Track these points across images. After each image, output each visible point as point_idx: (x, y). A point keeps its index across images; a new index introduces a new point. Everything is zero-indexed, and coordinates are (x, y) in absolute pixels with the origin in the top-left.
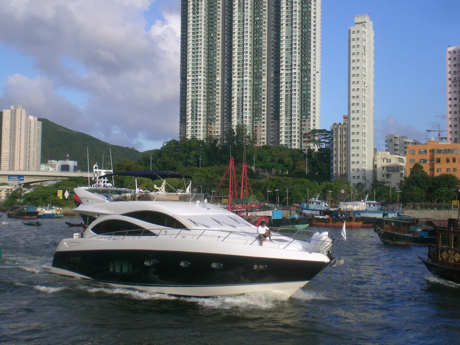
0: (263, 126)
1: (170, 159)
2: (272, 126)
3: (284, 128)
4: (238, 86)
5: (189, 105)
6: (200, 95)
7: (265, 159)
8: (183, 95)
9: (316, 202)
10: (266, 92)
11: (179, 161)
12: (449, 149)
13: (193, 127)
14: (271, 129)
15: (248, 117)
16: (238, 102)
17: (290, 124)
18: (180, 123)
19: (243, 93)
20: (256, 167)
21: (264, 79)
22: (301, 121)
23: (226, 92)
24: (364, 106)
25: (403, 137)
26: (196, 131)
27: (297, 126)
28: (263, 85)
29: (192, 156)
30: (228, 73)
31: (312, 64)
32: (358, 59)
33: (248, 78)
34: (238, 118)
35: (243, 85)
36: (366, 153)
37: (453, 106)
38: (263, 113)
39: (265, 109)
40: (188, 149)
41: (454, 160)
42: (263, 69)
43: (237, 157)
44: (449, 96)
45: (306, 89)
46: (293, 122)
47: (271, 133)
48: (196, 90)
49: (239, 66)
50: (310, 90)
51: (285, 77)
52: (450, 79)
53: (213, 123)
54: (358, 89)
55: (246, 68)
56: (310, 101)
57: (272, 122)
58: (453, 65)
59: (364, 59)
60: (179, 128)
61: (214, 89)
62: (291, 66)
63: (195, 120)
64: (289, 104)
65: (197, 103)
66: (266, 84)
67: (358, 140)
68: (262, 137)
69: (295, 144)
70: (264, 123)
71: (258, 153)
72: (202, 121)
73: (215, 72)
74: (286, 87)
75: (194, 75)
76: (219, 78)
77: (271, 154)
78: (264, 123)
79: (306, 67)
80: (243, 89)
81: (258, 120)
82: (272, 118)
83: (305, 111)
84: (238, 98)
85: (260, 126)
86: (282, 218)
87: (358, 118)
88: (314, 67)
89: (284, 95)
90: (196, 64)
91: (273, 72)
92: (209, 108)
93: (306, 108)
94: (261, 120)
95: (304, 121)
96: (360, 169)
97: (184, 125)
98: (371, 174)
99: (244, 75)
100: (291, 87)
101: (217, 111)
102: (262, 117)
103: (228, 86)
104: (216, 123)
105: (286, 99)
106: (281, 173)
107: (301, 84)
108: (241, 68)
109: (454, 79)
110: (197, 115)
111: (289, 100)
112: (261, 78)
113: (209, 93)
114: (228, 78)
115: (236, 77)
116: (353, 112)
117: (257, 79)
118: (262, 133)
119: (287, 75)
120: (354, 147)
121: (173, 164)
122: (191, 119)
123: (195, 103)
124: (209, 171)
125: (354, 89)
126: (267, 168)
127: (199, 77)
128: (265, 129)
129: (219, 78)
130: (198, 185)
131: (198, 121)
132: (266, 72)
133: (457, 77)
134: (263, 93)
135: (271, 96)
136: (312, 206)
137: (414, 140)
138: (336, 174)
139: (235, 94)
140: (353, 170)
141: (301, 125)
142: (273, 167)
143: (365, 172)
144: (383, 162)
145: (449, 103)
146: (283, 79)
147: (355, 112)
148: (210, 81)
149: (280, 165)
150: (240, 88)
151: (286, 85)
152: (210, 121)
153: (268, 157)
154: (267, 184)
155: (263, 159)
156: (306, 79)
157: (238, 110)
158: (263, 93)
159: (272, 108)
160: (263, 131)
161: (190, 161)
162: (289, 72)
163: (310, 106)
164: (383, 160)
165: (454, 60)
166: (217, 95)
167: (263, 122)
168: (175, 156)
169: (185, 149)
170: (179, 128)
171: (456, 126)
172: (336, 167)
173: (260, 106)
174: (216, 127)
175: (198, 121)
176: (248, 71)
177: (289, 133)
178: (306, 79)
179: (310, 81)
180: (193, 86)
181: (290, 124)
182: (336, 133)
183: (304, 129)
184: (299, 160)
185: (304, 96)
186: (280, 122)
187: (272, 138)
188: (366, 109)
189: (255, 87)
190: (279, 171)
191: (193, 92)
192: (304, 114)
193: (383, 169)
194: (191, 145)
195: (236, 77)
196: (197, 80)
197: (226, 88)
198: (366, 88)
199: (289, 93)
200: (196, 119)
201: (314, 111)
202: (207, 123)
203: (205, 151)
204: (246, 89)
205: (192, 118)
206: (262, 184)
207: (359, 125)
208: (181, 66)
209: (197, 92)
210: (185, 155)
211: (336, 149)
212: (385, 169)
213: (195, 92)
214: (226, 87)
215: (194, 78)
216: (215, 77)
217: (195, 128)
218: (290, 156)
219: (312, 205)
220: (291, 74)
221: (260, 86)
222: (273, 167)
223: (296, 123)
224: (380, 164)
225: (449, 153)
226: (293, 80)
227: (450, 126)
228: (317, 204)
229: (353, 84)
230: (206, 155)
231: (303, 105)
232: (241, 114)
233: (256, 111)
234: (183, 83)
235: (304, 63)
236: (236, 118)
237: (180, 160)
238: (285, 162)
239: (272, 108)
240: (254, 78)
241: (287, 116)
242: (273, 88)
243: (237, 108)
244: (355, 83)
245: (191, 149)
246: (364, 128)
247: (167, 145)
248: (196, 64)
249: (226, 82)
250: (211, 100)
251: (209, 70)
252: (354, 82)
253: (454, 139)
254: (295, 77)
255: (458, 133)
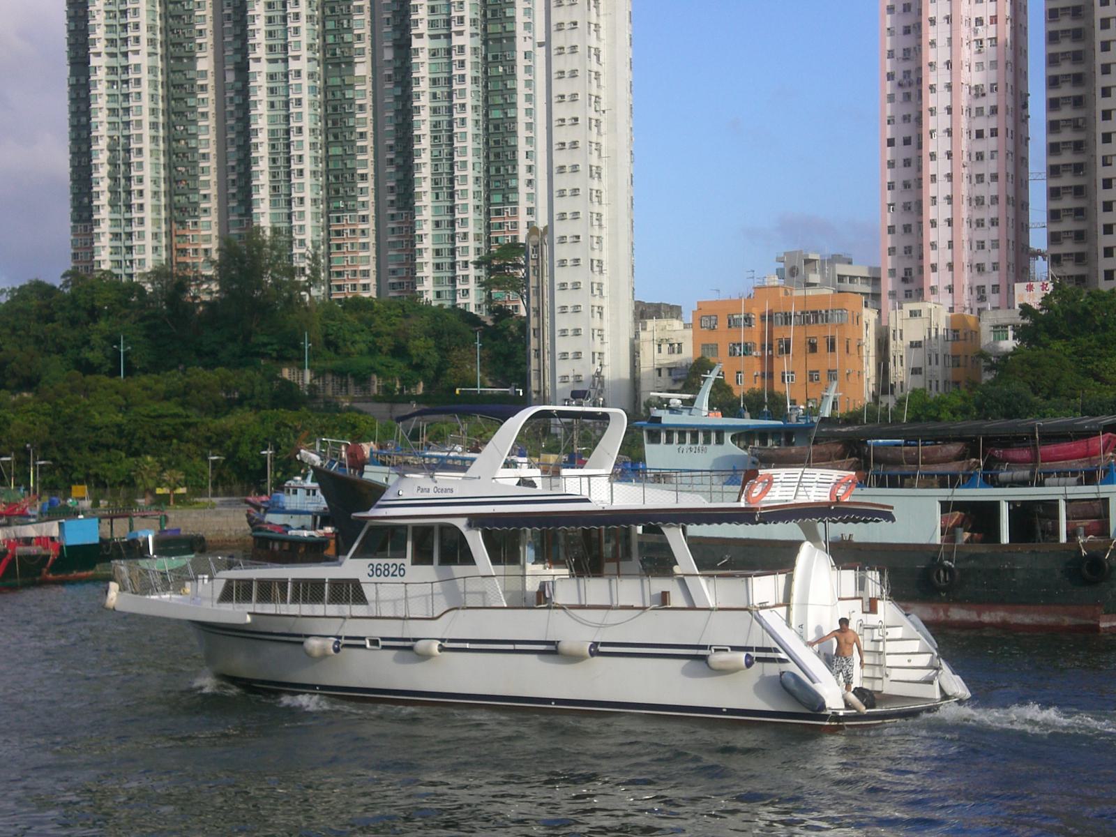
0: (363, 231)
1: (21, 350)
2: (393, 229)
3: (430, 237)
4: (272, 91)
5: (101, 156)
6: (139, 124)
7: (349, 344)
8: (79, 121)
9: (303, 488)
10: (368, 114)
11: (55, 357)
12: (816, 312)
13: (116, 236)
14: (390, 240)
15: (308, 202)
16: (273, 146)
17: (449, 222)
18: (74, 221)
19: (287, 118)
20: (318, 374)
21: (363, 69)
22: (488, 213)
23: (232, 112)
24: (595, 172)
25: (836, 259)
26: (130, 249)
27: (471, 229)
28: (357, 88)
29: (96, 338)
30: (238, 44)
31: (520, 18)
32: (574, 20)
33: (303, 63)
34: (274, 204)
35: (288, 87)
36: (606, 326)
37: (900, 163)
38: (360, 185)
39: (370, 171)
40: (84, 316)
41: (832, 346)
42: (356, 32)
43: (253, 339)
44: (888, 132)
45: (502, 102)
46: (457, 216)
47: (390, 253)
48: (125, 105)
49: (270, 20)
50: (514, 105)
51: (428, 61)
52: (890, 76)
53: (190, 222)
54: (576, 119)
55: (297, 30)
56: (515, 146)
57: (393, 216)
58: (900, 30)
59: (594, 20)
60: (72, 237)
61: (191, 102)
62: (448, 23)
63: (123, 209)
64: (444, 155)
65: (128, 151)
66: (368, 87)
67: (576, 286)
68: (361, 268)
69: (467, 290)
70: (364, 219)
71: (326, 325)
72: (148, 214)
73: (192, 39)
74: (434, 96)
75: (113, 50)
76: (205, 63)
77: (370, 327)
78: (364, 219)
79: (499, 28)
80: (287, 104)
81: (346, 209)
82: (392, 202)
83: (501, 178)
84: (272, 132)
85: (353, 231)
86: (97, 541)
87: (577, 213)
88: (528, 26)
89: (428, 124)
90: (121, 11)
91: (390, 44)
92: (175, 168)
93: (502, 169)
94: (355, 210)
95: (498, 212)
96: (583, 378)
97: (85, 227)
98: (626, 391)
99: (291, 53)
100: (450, 95)
101: (202, 178)
102: (360, 199)
103: (238, 92)
104: (202, 219)
105: (435, 138)
106: (401, 390)
107: (486, 86)
108: (278, 28)
109: (905, 77)
110: (129, 193)
111: (444, 140)
112: (351, 64)
113: (173, 117)
114: (236, 63)
115: (263, 60)
116: (562, 193)
117: (337, 69)
118: (361, 254)
119: (434, 53)
120: (565, 307)
121: (30, 367)
122: (108, 208)
123: (122, 152)
124: (145, 388)
125: (563, 120)
126: (353, 376)
127: (133, 60)
128: (371, 239)
129: (205, 63)
130: (22, 441)
131: (135, 214)
132: (366, 44)
133: (913, 70)
134: (358, 116)
135: (387, 129)
136: (290, 501)
137: (870, 269)
138: (538, 392)
139: (262, 119)
140: (564, 379)
141: (489, 226)
142: (373, 370)
143: (603, 386)
144: (660, 351)
145: (888, 153)
146: (423, 69)
147: (568, 193)
148: (174, 72)
149: (399, 364)
150: (279, 99)
151: (434, 90)
152: (180, 211)
153: (357, 337)
154: (242, 432)
155: (341, 344)
156: (501, 69)
157: (274, 175)
158: (358, 116)
159: (391, 170)
160: (364, 246)
161: (92, 354)
162: (441, 44)
163: (514, 163)
164: (659, 345)
165: (904, 11)
166: (200, 124)
167: (364, 216)
168: (38, 341)
169: (73, 312)
170: (72, 237)
171: (910, 231)
172: (539, 371)
173: (348, 162)
174: (203, 233)
175: (135, 214)
176: (304, 38)
177: (446, 253)
178: (501, 69)
179: (513, 76)
180: (111, 92)
181: (449, 222)
182: (538, 259)
183: (497, 239)
184: (457, 345)
185: (497, 127)
186: (417, 218)
187: (394, 272)
188: (604, 185)
189: (330, 97)
190: (395, 385)
191: (113, 111)
192: (497, 190)
193: (660, 375)
194: (93, 299)
195: (263, 60)
196: (126, 69)
197: (231, 99)
198: (603, 118)
199: (444, 118)
200: (129, 207)
201: (531, 177)
202: (169, 221)
203: (143, 319)
204: (299, 102)
205: (113, 205)
206: (228, 434)
207: (578, 237)
208: (70, 18)
209: (127, 110)
210: (76, 333)
211: (538, 312)
212: (665, 373)
213: (120, 112)
214: (232, 95)
215: (113, 62)
216: (193, 59)
217: (124, 238)
218: (428, 334)
219: (293, 497)
220: (449, 52)
221: (346, 92)
222: (373, 370)
223: (471, 221)
224: (651, 358)
225: (817, 321)
226: (455, 72)
227: (891, 230)
228: (308, 494)
229: (560, 102)
230: (144, 333)
231: (492, 158)
232: (283, 190)
233: (336, 177)
234: (78, 80)
235: (494, 13)
236: (267, 202)
237: (58, 353)
238: (414, 352)
239: (393, 170)
240: (325, 62)
241: (437, 198)
242: (391, 100)
243: (271, 168)
244: (567, 99)
245: (94, 314)
246: (596, 246)
247: (14, 299)
248: (121, 11)
249: (230, 77)
250: (178, 141)
251: (171, 36)
252: (563, 97)
253: (901, 273)
254: (462, 64)
255: (913, 253)
